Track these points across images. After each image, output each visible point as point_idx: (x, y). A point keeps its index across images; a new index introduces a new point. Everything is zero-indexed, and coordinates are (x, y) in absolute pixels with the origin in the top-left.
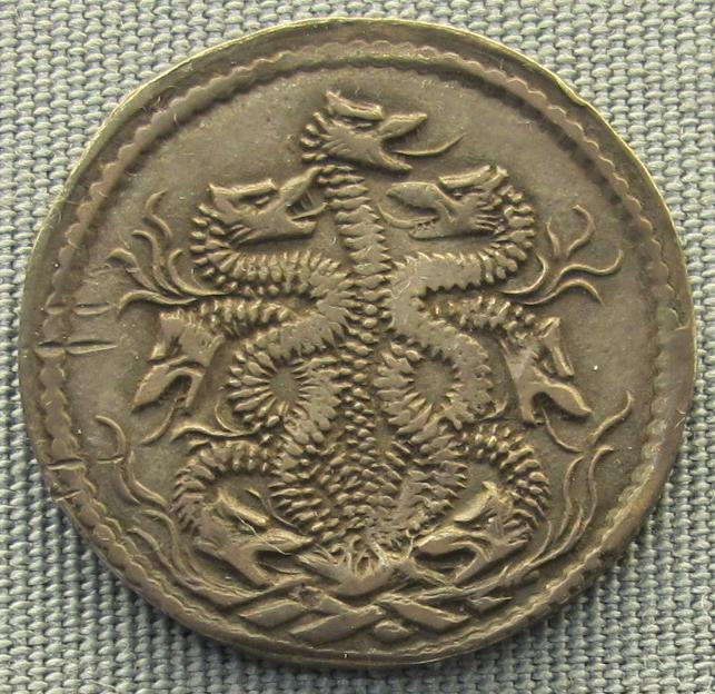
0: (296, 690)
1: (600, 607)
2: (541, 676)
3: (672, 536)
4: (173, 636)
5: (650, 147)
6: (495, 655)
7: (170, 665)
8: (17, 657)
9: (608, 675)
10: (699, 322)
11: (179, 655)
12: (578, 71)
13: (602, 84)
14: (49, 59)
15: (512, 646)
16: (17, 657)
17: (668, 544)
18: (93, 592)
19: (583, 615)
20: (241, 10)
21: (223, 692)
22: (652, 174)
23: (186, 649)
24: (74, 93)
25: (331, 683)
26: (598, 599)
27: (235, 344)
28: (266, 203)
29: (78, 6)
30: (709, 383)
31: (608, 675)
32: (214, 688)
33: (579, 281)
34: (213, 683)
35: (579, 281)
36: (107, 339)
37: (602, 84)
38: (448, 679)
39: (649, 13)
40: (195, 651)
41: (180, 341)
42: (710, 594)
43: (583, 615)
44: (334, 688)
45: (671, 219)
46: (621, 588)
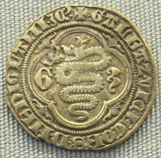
0: (71, 157)
3: (141, 134)
4: (19, 128)
6: (123, 144)
7: (29, 147)
8: (26, 153)
9: (143, 138)
10: (158, 89)
14: (5, 24)
15: (127, 142)
16: (26, 153)
21: (62, 157)
22: (148, 44)
25: (99, 155)
28: (107, 111)
31: (143, 138)
32: (59, 156)
34: (49, 151)
39: (132, 8)
41: (56, 75)
42: (160, 129)
44: (81, 156)
45: (154, 60)
46: (146, 131)
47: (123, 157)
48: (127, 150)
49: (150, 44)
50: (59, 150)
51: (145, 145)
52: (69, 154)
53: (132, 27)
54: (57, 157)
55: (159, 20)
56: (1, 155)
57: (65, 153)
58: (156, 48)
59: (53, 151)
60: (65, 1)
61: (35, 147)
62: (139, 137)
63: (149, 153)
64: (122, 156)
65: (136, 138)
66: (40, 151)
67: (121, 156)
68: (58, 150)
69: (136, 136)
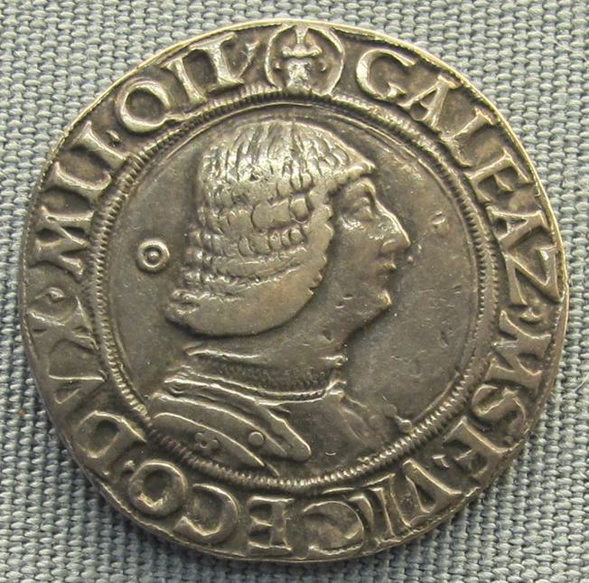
1: (449, 539)
2: (553, 424)
5: (556, 91)
11: (133, 567)
12: (132, 42)
13: (495, 32)
14: (23, 93)
15: (420, 548)
17: (541, 452)
18: (66, 530)
19: (435, 544)
20: (372, 8)
23: (141, 551)
24: (26, 130)
26: (448, 533)
27: (178, 321)
29: (537, 9)
30: (585, 326)
33: (176, 392)
35: (176, 392)
36: (437, 188)
37: (495, 32)
38: (336, 576)
40: (149, 554)
43: (435, 544)
47: (449, 581)
48: (495, 514)
49: (556, 200)
50: (161, 557)
51: (497, 21)
52: (195, 571)
53: (497, 129)
54: (182, 580)
55: (583, 72)
56: (5, 34)
57: (193, 567)
58: (540, 506)
59: (144, 555)
60: (560, 2)
61: (116, 541)
62: (443, 552)
63: (561, 533)
64: (445, 575)
65: (465, 523)
66: (103, 551)
67: (459, 558)
68: (159, 554)
69: (419, 554)
